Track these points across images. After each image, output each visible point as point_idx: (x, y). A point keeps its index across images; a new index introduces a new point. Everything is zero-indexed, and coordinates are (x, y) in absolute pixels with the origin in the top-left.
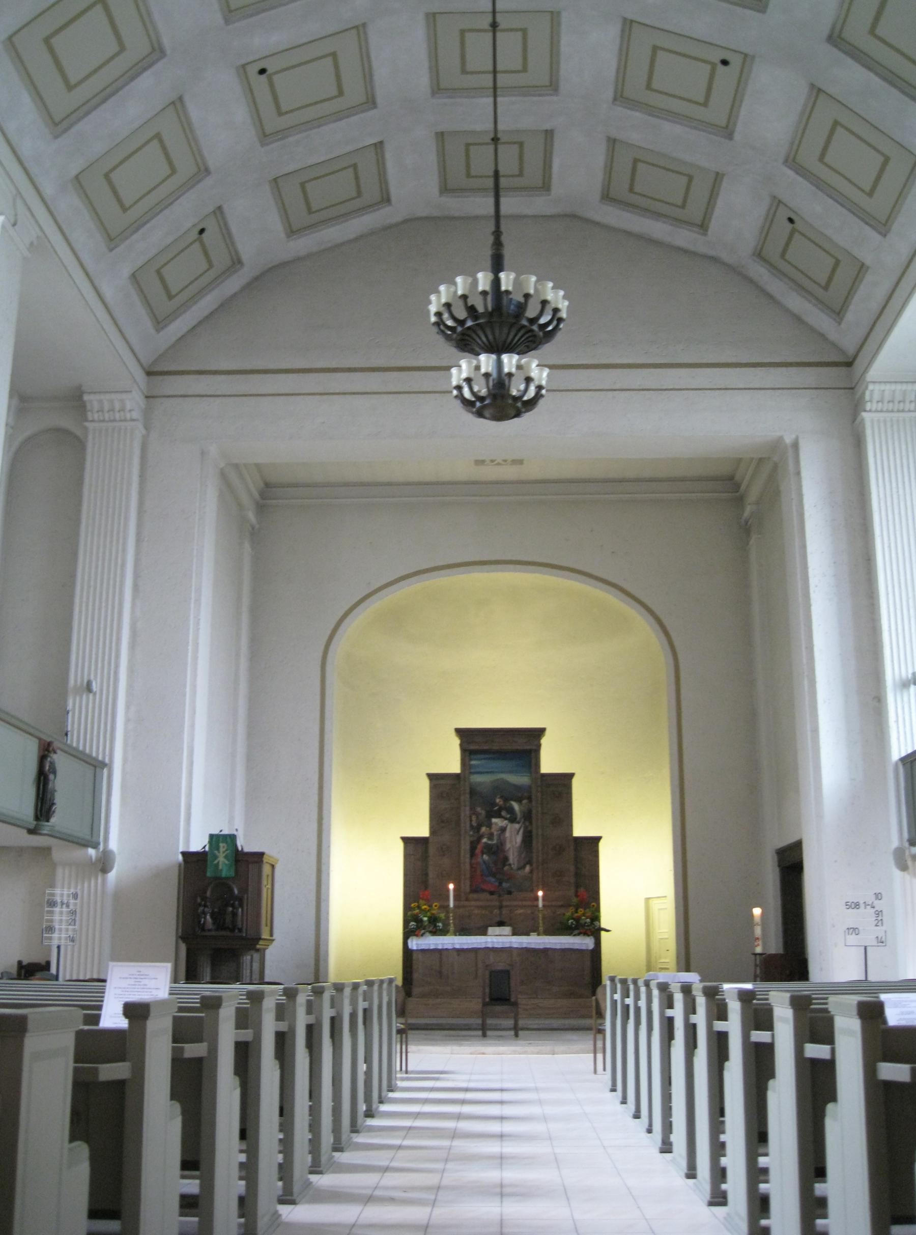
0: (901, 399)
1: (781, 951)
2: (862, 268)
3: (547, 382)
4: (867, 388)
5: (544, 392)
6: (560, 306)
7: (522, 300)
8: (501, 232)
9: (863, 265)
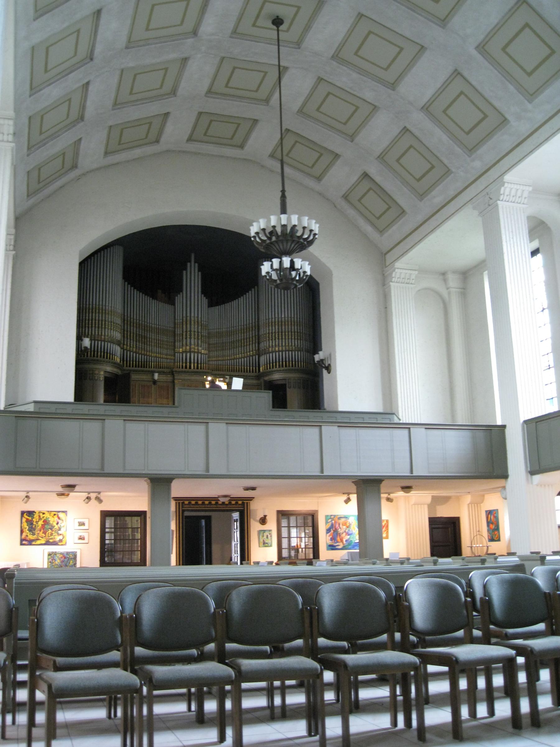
0: (399, 277)
1: (271, 392)
2: (448, 172)
3: (319, 231)
4: (394, 270)
5: (317, 236)
6: (313, 229)
7: (243, 562)
8: (285, 191)
9: (449, 170)
